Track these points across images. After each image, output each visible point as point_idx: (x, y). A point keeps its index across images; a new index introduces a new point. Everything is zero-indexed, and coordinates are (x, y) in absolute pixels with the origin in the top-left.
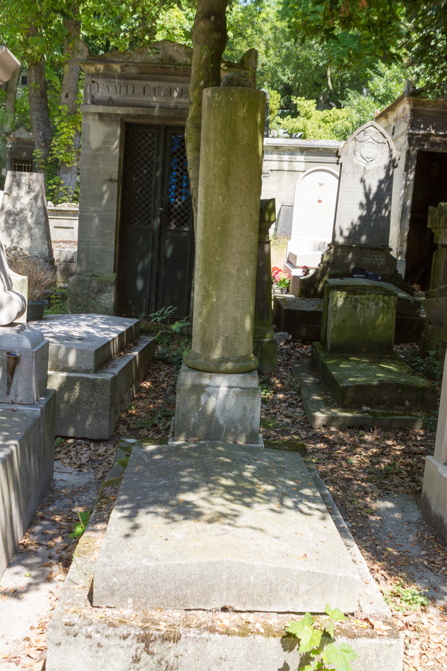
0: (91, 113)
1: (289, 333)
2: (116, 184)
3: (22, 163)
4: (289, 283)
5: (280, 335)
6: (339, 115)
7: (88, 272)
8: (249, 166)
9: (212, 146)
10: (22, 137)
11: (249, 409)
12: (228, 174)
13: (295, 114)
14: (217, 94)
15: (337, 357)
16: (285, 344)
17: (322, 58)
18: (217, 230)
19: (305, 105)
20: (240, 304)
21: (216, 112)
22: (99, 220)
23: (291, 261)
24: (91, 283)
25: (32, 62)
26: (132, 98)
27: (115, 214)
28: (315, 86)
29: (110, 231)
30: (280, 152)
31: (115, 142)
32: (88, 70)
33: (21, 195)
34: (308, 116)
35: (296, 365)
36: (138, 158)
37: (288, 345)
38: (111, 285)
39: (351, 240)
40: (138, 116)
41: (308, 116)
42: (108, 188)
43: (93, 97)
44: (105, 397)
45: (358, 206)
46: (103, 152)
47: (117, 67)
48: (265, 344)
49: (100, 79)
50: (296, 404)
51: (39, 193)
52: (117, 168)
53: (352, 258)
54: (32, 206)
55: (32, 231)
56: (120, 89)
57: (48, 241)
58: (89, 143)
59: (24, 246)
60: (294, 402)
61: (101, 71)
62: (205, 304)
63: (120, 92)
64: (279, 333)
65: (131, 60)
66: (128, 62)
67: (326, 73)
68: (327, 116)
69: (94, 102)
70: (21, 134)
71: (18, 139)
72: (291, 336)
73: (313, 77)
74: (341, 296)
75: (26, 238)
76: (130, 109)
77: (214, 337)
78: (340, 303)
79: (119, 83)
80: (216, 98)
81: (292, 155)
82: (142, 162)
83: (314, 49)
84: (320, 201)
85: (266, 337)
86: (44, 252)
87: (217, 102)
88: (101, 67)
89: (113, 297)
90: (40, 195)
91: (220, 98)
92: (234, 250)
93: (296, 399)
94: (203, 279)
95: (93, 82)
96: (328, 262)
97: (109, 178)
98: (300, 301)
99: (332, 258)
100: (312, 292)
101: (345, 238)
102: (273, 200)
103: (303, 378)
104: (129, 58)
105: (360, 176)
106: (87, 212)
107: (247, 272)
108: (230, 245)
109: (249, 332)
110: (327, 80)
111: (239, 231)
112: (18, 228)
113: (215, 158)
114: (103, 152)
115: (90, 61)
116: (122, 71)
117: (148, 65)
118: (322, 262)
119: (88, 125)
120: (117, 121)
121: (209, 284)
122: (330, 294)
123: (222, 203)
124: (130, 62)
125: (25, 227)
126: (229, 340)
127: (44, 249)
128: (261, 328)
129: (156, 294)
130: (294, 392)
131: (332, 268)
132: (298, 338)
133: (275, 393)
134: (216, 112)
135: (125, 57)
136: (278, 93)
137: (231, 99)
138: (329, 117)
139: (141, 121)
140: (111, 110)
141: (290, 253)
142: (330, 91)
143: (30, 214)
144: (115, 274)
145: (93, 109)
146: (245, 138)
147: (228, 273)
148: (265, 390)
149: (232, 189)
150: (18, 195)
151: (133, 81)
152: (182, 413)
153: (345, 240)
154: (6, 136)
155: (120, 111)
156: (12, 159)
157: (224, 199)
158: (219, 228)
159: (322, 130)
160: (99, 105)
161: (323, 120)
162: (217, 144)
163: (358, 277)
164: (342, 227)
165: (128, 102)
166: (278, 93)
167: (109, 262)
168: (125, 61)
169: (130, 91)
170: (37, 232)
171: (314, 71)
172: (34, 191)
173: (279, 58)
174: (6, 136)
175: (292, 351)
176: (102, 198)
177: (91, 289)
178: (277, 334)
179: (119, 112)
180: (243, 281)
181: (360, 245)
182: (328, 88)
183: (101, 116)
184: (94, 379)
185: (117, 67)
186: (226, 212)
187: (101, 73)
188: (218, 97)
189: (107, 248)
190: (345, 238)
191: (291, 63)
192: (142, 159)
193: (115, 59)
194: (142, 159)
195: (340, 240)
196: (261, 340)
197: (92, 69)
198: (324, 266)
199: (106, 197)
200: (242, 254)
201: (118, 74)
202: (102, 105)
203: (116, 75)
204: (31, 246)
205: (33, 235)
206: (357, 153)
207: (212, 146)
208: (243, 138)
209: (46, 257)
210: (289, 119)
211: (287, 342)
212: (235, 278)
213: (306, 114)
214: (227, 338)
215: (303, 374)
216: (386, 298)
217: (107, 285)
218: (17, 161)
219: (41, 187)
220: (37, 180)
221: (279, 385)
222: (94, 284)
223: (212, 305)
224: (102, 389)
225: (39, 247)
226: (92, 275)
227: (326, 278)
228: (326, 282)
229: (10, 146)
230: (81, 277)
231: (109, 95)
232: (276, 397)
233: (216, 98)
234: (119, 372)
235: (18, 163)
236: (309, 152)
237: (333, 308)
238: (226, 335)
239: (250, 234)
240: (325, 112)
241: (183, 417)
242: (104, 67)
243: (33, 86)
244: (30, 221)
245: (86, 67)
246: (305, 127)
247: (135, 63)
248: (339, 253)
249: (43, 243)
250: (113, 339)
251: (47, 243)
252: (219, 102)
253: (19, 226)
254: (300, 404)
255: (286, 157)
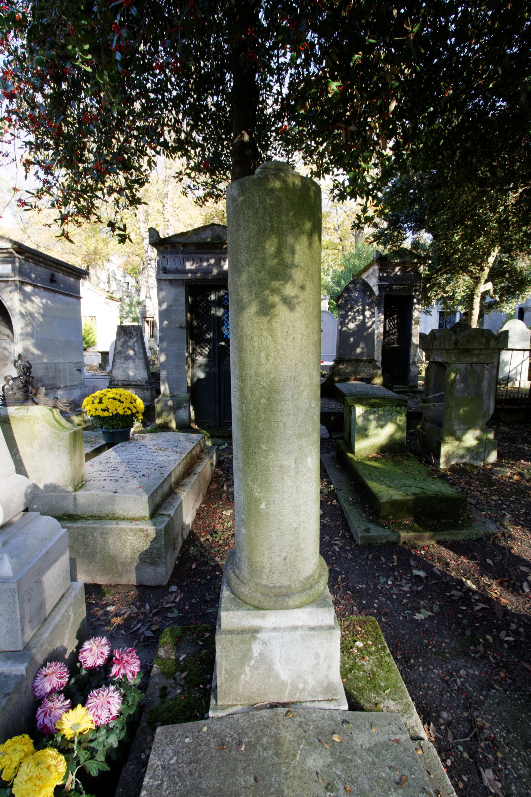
2: (185, 330)
11: (322, 656)
92: (289, 432)
108: (281, 425)
114: (174, 308)
126: (288, 561)
129: (219, 406)
152: (226, 670)
216: (398, 408)
238: (284, 555)
241: (228, 674)
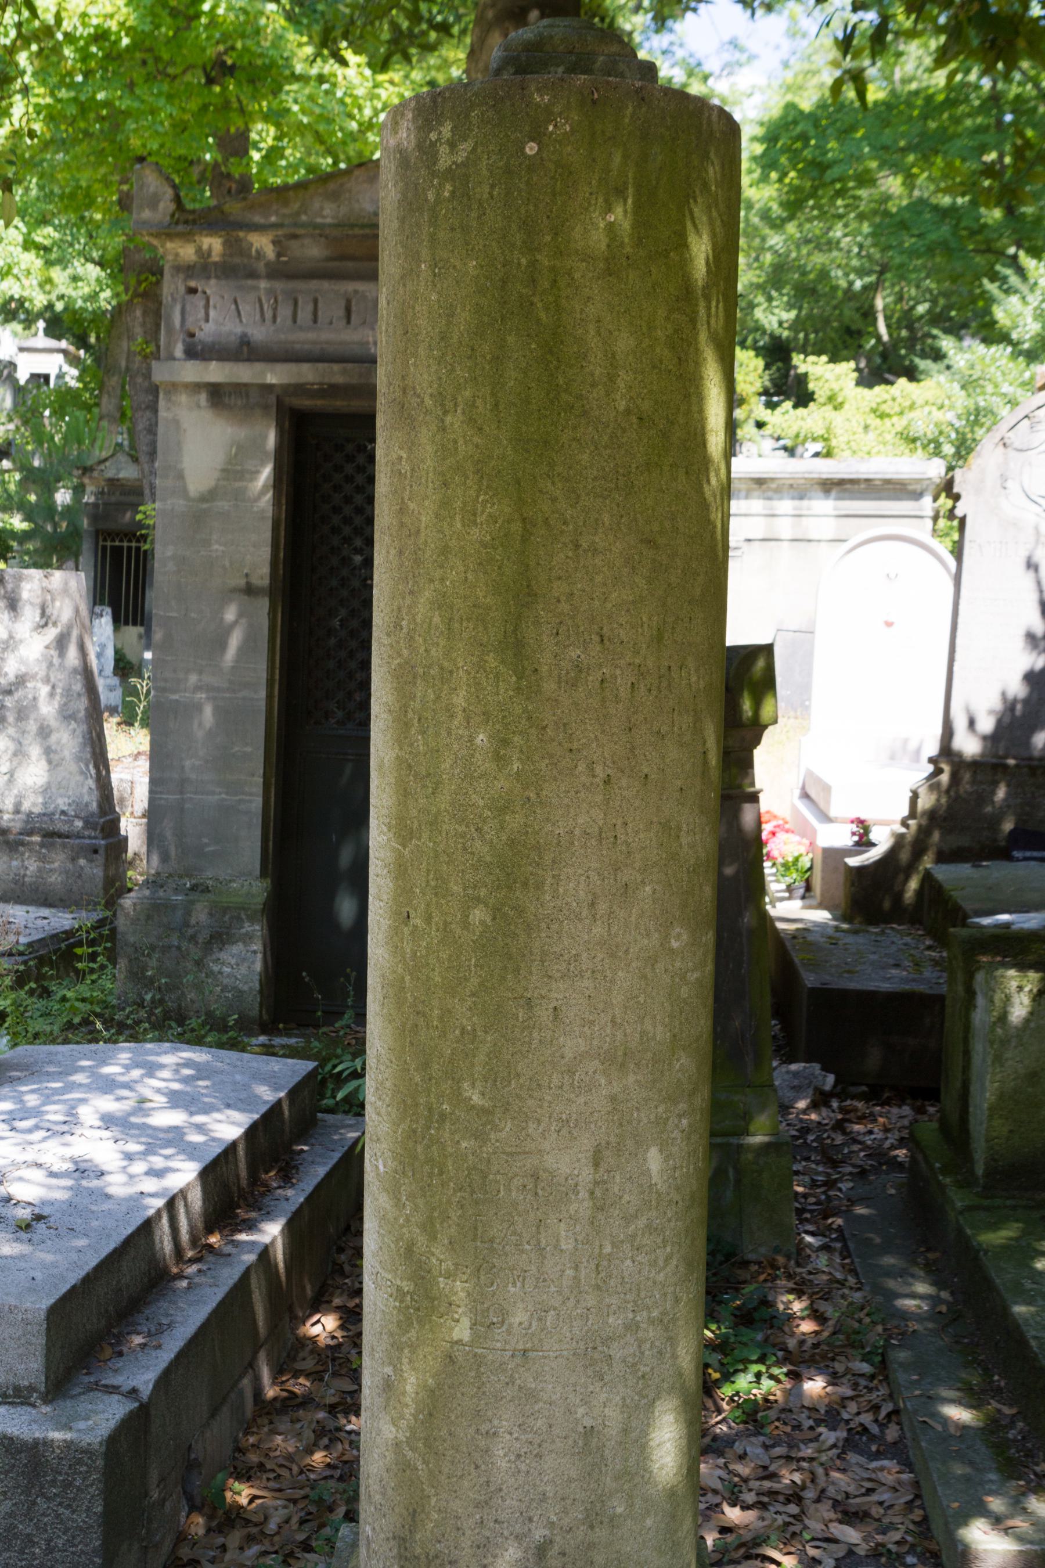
0: (187, 386)
1: (826, 1069)
2: (264, 603)
3: (121, 541)
4: (810, 869)
5: (796, 1074)
6: (914, 397)
7: (181, 877)
8: (650, 542)
9: (425, 435)
10: (121, 475)
12: (522, 595)
13: (803, 398)
14: (446, 130)
15: (1014, 1208)
16: (814, 1106)
17: (861, 272)
18: (466, 925)
19: (828, 375)
20: (616, 1351)
21: (443, 235)
22: (214, 715)
23: (813, 794)
24: (188, 913)
25: (135, 290)
26: (311, 336)
27: (263, 694)
28: (847, 338)
29: (249, 749)
30: (770, 494)
31: (258, 472)
32: (177, 255)
33: (18, 637)
34: (834, 402)
35: (860, 1210)
36: (336, 520)
37: (825, 1111)
38: (251, 919)
39: (1002, 745)
40: (332, 390)
41: (834, 402)
42: (240, 615)
43: (192, 335)
44: (80, 1518)
45: (1020, 642)
46: (223, 505)
47: (262, 243)
48: (750, 1156)
49: (213, 282)
50: (875, 1429)
51: (70, 627)
52: (265, 553)
53: (1005, 800)
54: (51, 665)
55: (54, 738)
56: (275, 309)
57: (97, 767)
58: (180, 476)
59: (30, 782)
60: (866, 1419)
61: (216, 258)
62: (413, 1348)
63: (274, 317)
64: (794, 1067)
65: (304, 218)
66: (296, 225)
67: (872, 306)
68: (885, 402)
69: (193, 353)
70: (119, 470)
71: (111, 481)
72: (831, 1079)
73: (841, 314)
74: (1020, 988)
75: (34, 758)
76: (305, 367)
77: (466, 1543)
78: (1020, 1009)
79: (270, 292)
80: (444, 149)
81: (801, 498)
82: (347, 530)
83: (841, 250)
84: (889, 624)
85: (752, 1128)
86: (86, 798)
87: (449, 174)
88: (214, 244)
89: (260, 956)
90: (75, 633)
91: (465, 148)
92: (571, 1045)
93: (876, 1408)
94: (398, 1204)
95: (193, 291)
96: (932, 815)
97: (242, 582)
98: (850, 939)
99: (944, 800)
100: (887, 905)
101: (985, 738)
102: (767, 650)
103: (891, 1284)
104: (298, 214)
105: (1023, 554)
106: (175, 692)
107: (654, 1160)
108: (544, 1015)
109: (671, 1493)
110: (875, 319)
111: (598, 930)
112: (11, 731)
113: (445, 503)
114: (223, 505)
115: (180, 228)
116: (279, 255)
117: (357, 231)
118: (913, 813)
119: (176, 422)
120: (266, 407)
121: (433, 1237)
122: (980, 977)
123: (489, 766)
124: (303, 225)
125: (32, 726)
127: (85, 790)
128: (736, 1098)
130: (865, 1368)
131: (946, 832)
132: (858, 1084)
133: (796, 1376)
134: (443, 235)
135: (286, 211)
136: (757, 356)
137: (531, 149)
138: (890, 403)
139: (339, 404)
140: (244, 373)
141: (809, 774)
142: (884, 344)
143: (44, 690)
144: (267, 883)
145: (192, 372)
146: (624, 378)
147: (536, 1178)
148: (755, 1368)
149: (549, 687)
150: (11, 637)
151: (314, 284)
153: (985, 747)
154: (84, 474)
155: (274, 376)
156: (97, 532)
157: (505, 742)
158: (478, 915)
159: (872, 435)
160: (211, 359)
161: (874, 411)
162: (455, 421)
163: (1026, 859)
164: (973, 707)
165: (297, 346)
166: (757, 356)
167: (248, 847)
168: (286, 222)
169: (305, 314)
170: (68, 740)
171: (842, 302)
172: (55, 624)
173: (758, 272)
174: (84, 474)
175: (839, 1139)
176: (223, 646)
177: (190, 931)
178: (784, 1068)
179: (271, 379)
180: (628, 1220)
181: (1031, 759)
182: (879, 338)
183: (218, 395)
184: (36, 1442)
185: (262, 243)
186: (515, 821)
187: (215, 264)
188: (452, 145)
189: (240, 801)
190: (985, 738)
191: (786, 283)
192: (347, 521)
193: (258, 219)
194: (347, 521)
195: (968, 745)
196: (734, 1140)
197: (187, 252)
198: (920, 827)
199: (235, 641)
200: (617, 1060)
201: (268, 264)
202: (220, 359)
203: (261, 267)
204: (49, 783)
205: (55, 752)
206: (1009, 484)
207: (425, 435)
208: (612, 378)
209: (92, 815)
210: (787, 412)
211: (821, 1100)
212: (581, 1205)
213: (831, 399)
214: (542, 1550)
215: (889, 1260)
217: (239, 919)
218: (109, 534)
219: (77, 611)
220: (65, 591)
221: (807, 1327)
222: (201, 915)
223: (450, 1359)
224: (67, 1485)
225: (73, 784)
226: (194, 888)
227: (927, 862)
228: (928, 877)
229: (92, 500)
230: (161, 893)
231: (239, 330)
232: (800, 1394)
233: (444, 149)
234: (164, 1380)
235: (113, 540)
236: (845, 490)
237: (992, 1031)
238: (539, 1533)
239: (666, 937)
240: (880, 391)
242: (224, 244)
243: (138, 349)
244: (48, 709)
245: (169, 245)
246: (828, 430)
247: (316, 226)
248: (966, 785)
249: (82, 773)
250: (171, 1204)
251: (93, 771)
252: (460, 176)
253: (16, 726)
254: (892, 1433)
255: (785, 505)
